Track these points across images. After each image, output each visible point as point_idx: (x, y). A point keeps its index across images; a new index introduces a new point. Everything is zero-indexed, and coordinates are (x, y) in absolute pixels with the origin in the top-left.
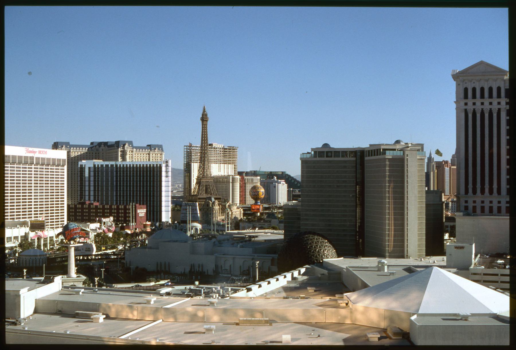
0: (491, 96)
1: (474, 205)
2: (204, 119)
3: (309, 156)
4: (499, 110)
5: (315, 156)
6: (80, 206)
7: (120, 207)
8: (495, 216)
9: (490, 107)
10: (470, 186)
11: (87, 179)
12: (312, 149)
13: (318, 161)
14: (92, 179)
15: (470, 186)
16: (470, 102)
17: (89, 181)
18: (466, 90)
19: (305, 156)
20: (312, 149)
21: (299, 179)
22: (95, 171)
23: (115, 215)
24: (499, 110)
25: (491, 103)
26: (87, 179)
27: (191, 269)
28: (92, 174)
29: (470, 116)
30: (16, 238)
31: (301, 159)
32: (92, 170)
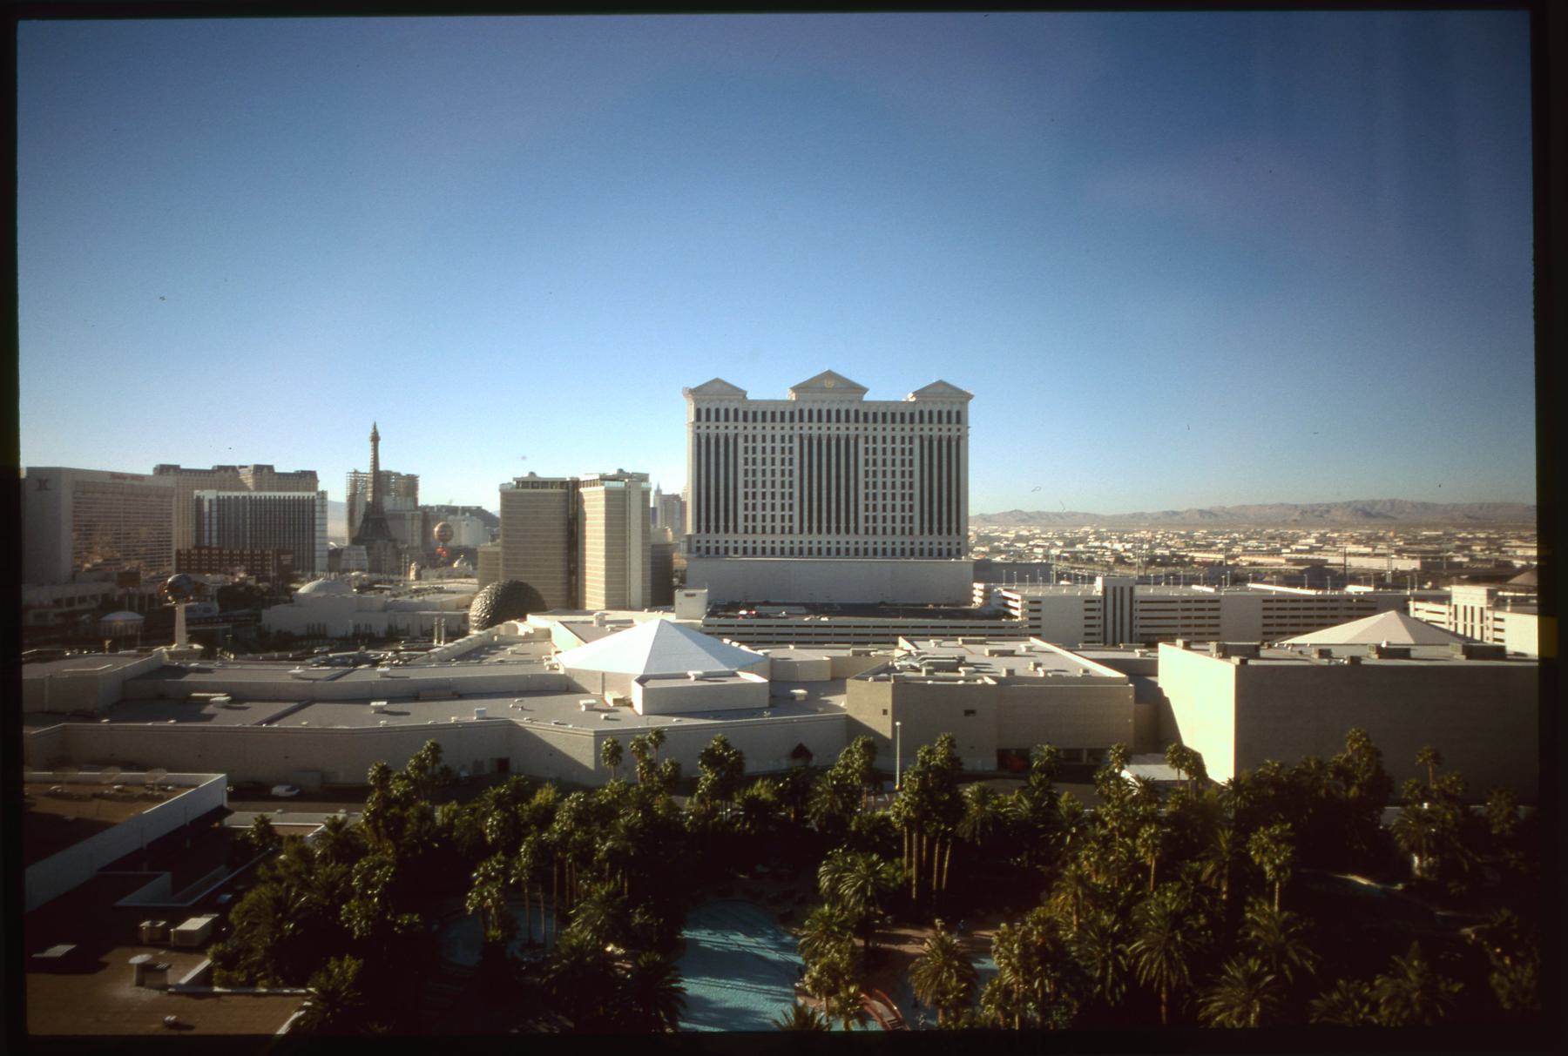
0: (773, 420)
1: (810, 546)
2: (375, 439)
3: (509, 487)
4: (736, 435)
5: (517, 487)
6: (196, 551)
7: (256, 552)
8: (936, 559)
9: (726, 431)
10: (926, 525)
11: (207, 515)
12: (515, 479)
13: (521, 494)
14: (214, 515)
15: (926, 525)
16: (703, 424)
17: (210, 517)
18: (959, 421)
19: (505, 487)
20: (515, 479)
21: (498, 515)
22: (218, 505)
23: (249, 563)
24: (736, 435)
25: (847, 429)
26: (207, 515)
27: (355, 630)
28: (215, 508)
29: (703, 441)
30: (94, 597)
31: (501, 490)
32: (214, 502)
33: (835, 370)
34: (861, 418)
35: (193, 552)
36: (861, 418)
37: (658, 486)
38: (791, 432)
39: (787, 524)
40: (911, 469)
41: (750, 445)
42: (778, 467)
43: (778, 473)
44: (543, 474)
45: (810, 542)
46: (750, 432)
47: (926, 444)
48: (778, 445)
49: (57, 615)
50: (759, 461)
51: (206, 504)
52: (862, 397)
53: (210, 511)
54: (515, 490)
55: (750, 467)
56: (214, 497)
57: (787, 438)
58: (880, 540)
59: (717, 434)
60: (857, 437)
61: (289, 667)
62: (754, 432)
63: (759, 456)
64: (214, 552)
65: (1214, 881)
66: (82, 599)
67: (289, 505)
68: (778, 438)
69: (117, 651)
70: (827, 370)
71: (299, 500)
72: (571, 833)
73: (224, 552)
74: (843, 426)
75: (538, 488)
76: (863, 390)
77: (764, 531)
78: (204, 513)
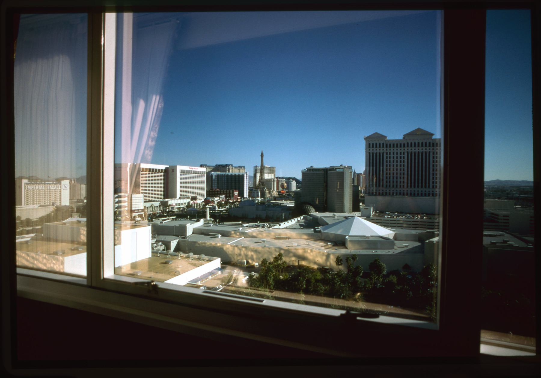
2: (262, 155)
3: (305, 171)
12: (306, 168)
14: (216, 179)
16: (371, 149)
17: (215, 180)
19: (303, 171)
29: (371, 155)
30: (185, 203)
31: (302, 172)
32: (216, 176)
33: (421, 128)
34: (385, 146)
35: (210, 191)
36: (385, 146)
37: (355, 170)
38: (404, 151)
39: (402, 184)
40: (401, 164)
41: (388, 156)
42: (399, 164)
43: (399, 166)
44: (315, 166)
45: (418, 191)
46: (388, 151)
47: (409, 154)
48: (399, 156)
49: (176, 208)
50: (392, 162)
51: (214, 176)
52: (432, 137)
53: (215, 178)
54: (307, 172)
55: (388, 164)
56: (216, 174)
57: (402, 153)
58: (398, 190)
59: (376, 152)
60: (430, 152)
61: (237, 227)
62: (390, 151)
63: (392, 160)
64: (216, 192)
65: (254, 296)
66: (182, 204)
67: (238, 177)
68: (399, 153)
69: (191, 219)
70: (418, 128)
71: (237, 175)
72: (251, 277)
73: (224, 191)
74: (413, 148)
75: (314, 171)
76: (433, 135)
77: (400, 187)
78: (213, 179)
